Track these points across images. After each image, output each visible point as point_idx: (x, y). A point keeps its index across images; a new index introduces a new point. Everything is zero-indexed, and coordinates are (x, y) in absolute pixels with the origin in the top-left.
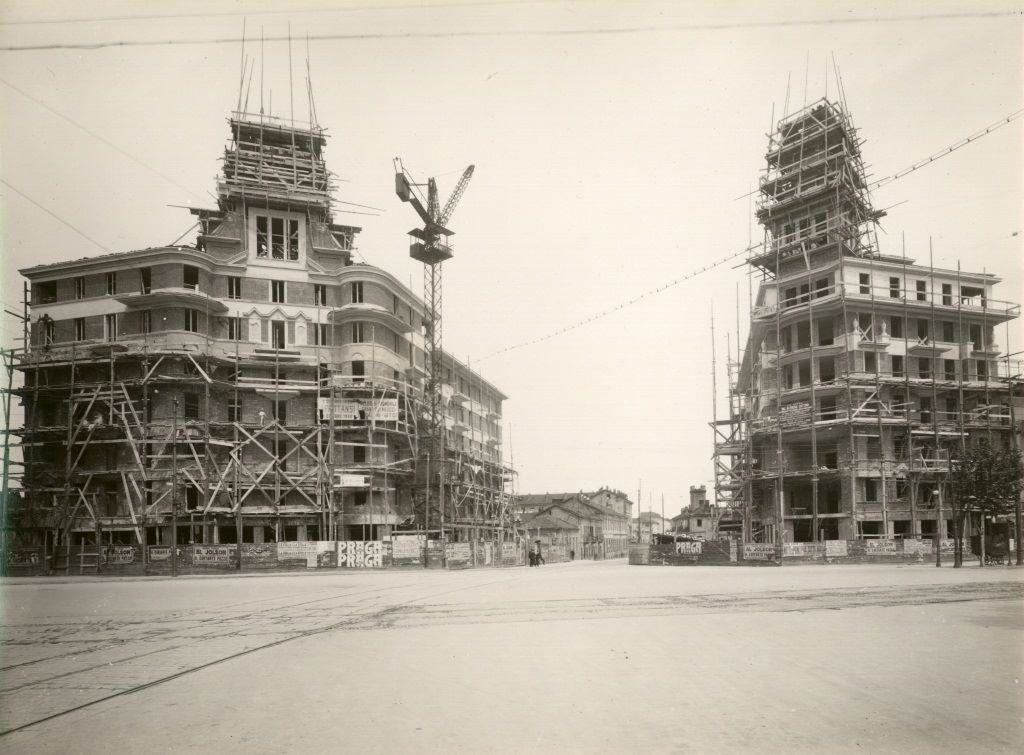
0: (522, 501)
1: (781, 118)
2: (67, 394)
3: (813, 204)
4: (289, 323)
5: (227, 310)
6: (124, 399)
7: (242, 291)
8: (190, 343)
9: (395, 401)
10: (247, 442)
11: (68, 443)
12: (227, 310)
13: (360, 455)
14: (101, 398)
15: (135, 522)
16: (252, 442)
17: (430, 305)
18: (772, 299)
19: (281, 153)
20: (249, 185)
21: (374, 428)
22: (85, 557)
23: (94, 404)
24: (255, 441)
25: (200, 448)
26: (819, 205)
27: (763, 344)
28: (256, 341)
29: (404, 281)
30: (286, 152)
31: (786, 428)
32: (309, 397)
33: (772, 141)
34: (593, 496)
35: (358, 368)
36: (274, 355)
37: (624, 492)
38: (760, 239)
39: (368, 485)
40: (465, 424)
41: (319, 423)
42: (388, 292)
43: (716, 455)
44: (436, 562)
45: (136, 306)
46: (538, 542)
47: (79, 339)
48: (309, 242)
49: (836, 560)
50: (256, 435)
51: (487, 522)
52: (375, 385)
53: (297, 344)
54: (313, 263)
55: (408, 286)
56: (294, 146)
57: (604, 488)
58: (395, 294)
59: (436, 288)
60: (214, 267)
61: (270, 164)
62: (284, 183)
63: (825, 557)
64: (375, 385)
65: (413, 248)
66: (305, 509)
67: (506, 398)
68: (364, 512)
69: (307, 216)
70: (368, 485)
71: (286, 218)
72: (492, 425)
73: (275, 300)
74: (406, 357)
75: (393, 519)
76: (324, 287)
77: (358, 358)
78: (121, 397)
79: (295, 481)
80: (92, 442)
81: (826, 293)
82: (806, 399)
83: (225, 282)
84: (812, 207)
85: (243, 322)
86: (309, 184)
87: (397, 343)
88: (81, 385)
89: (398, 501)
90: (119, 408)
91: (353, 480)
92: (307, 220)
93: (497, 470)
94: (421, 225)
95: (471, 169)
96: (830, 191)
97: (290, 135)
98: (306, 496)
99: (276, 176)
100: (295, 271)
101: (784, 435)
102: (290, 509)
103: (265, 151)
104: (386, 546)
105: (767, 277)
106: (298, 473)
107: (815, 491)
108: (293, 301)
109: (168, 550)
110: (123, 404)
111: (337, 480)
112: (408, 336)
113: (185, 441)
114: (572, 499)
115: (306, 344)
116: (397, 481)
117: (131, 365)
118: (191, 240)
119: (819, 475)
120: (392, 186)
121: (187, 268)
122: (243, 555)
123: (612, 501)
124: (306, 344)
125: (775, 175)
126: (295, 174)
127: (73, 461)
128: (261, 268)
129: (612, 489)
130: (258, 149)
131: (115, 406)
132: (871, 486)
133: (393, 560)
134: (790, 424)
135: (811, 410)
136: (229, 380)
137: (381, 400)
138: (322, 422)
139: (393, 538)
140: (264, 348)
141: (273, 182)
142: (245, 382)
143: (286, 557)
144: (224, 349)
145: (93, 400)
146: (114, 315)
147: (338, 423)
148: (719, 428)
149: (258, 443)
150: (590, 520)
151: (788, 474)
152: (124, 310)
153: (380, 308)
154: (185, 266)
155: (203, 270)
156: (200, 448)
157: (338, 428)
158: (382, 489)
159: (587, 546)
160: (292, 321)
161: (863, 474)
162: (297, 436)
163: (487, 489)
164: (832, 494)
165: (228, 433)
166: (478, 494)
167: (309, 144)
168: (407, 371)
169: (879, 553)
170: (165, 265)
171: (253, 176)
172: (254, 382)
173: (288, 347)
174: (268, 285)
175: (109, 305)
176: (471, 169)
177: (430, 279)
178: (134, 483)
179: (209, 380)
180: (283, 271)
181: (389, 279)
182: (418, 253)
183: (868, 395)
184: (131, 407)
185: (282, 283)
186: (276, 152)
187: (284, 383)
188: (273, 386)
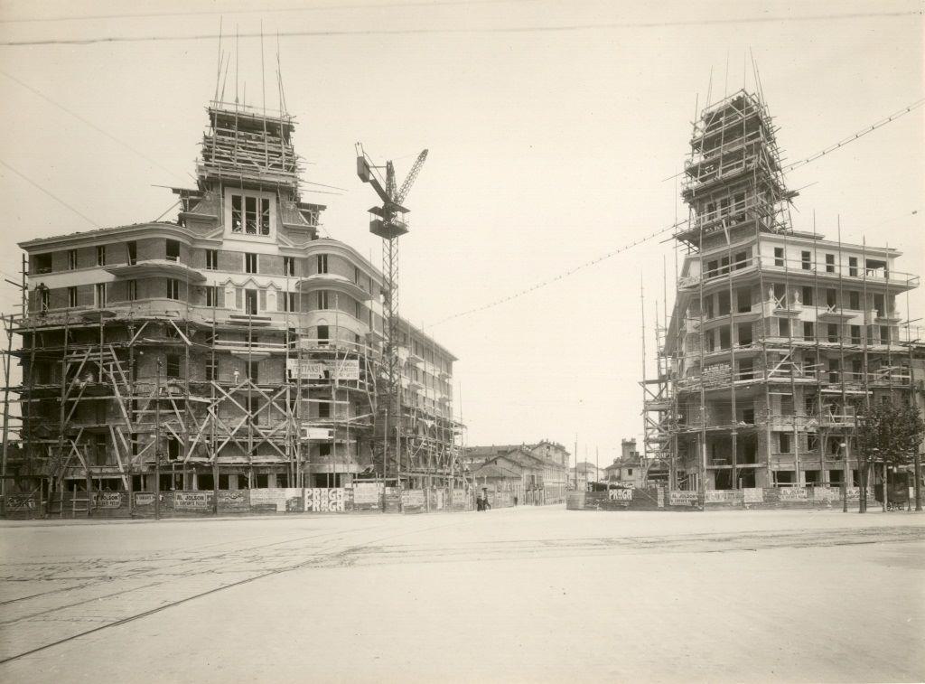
0: (470, 453)
2: (61, 355)
5: (205, 280)
9: (357, 362)
10: (223, 399)
11: (62, 399)
13: (324, 410)
17: (388, 276)
18: (696, 270)
25: (181, 404)
26: (738, 186)
27: (688, 312)
28: (232, 308)
29: (366, 256)
32: (278, 358)
33: (696, 128)
34: (534, 448)
35: (323, 332)
38: (685, 216)
39: (332, 437)
40: (419, 383)
43: (645, 411)
44: (393, 507)
46: (485, 489)
47: (72, 306)
48: (279, 219)
49: (753, 506)
50: (231, 393)
51: (439, 471)
52: (339, 347)
54: (284, 238)
55: (368, 259)
56: (266, 132)
57: (545, 441)
58: (357, 268)
60: (194, 241)
61: (243, 148)
62: (256, 165)
63: (743, 503)
64: (339, 347)
66: (275, 459)
67: (456, 359)
68: (328, 462)
70: (332, 437)
71: (259, 197)
72: (443, 383)
73: (248, 271)
75: (354, 468)
76: (292, 260)
78: (110, 358)
81: (744, 265)
82: (727, 362)
83: (204, 255)
84: (732, 188)
85: (220, 291)
86: (280, 166)
87: (357, 309)
88: (73, 347)
90: (107, 368)
92: (278, 199)
93: (448, 425)
94: (380, 204)
95: (425, 153)
96: (748, 173)
99: (249, 159)
100: (266, 245)
103: (239, 137)
104: (348, 492)
108: (264, 272)
110: (111, 364)
111: (304, 433)
113: (168, 398)
115: (276, 310)
117: (118, 329)
118: (173, 217)
119: (738, 430)
120: (353, 168)
121: (169, 241)
122: (219, 500)
123: (552, 452)
124: (276, 310)
125: (698, 159)
126: (267, 158)
127: (66, 415)
128: (236, 242)
130: (233, 135)
132: (784, 440)
133: (354, 505)
136: (207, 342)
138: (291, 381)
139: (355, 485)
141: (246, 165)
142: (221, 345)
143: (258, 502)
144: (202, 315)
145: (84, 361)
146: (103, 284)
147: (305, 381)
148: (648, 386)
149: (233, 400)
150: (532, 469)
151: (711, 428)
153: (343, 279)
156: (181, 404)
160: (264, 289)
161: (778, 428)
164: (750, 448)
165: (206, 391)
167: (279, 130)
169: (792, 500)
171: (229, 159)
173: (260, 313)
175: (100, 275)
176: (425, 153)
178: (121, 435)
179: (189, 343)
182: (377, 228)
183: (782, 357)
184: (119, 367)
185: (254, 256)
186: (250, 138)
187: (256, 346)
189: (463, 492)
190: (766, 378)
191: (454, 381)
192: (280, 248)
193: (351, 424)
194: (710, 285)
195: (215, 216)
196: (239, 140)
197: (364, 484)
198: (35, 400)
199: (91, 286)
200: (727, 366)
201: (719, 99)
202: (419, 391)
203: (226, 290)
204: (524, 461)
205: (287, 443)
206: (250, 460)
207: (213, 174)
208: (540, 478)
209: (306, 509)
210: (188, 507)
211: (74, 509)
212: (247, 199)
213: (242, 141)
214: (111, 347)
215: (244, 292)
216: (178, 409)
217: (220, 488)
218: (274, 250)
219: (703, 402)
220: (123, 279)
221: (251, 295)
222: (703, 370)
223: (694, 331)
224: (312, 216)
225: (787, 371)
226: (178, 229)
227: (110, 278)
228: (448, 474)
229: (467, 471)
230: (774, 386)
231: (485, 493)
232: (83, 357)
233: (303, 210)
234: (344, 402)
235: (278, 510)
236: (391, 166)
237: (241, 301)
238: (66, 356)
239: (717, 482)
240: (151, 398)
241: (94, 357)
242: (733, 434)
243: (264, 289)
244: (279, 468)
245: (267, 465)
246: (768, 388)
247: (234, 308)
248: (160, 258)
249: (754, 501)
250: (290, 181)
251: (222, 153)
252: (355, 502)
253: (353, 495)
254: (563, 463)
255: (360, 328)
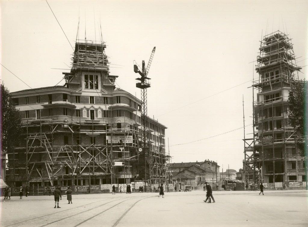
0: (174, 166)
1: (265, 35)
2: (25, 136)
3: (274, 67)
4: (96, 111)
5: (76, 107)
6: (45, 138)
7: (81, 100)
8: (66, 120)
9: (132, 136)
10: (84, 151)
11: (27, 153)
12: (76, 107)
13: (120, 155)
14: (37, 138)
15: (50, 179)
16: (85, 151)
17: (143, 101)
18: (262, 99)
19: (92, 53)
20: (83, 65)
21: (125, 146)
22: (39, 190)
23: (35, 140)
24: (86, 151)
25: (70, 154)
26: (276, 68)
27: (258, 114)
28: (86, 117)
29: (134, 94)
30: (94, 52)
31: (265, 144)
32: (104, 136)
33: (261, 43)
34: (201, 164)
35: (119, 126)
36: (92, 122)
37: (215, 161)
38: (257, 78)
39: (123, 165)
40: (133, 107)
41: (107, 145)
42: (127, 98)
43: (245, 152)
44: (149, 190)
45: (47, 107)
46: (180, 184)
47: (27, 118)
48: (102, 83)
49: (278, 189)
50: (86, 149)
51: (161, 176)
52: (125, 131)
53: (98, 118)
54: (103, 90)
55: (134, 95)
56: (96, 50)
57: (207, 160)
58: (130, 99)
59: (145, 98)
60: (72, 93)
61: (88, 57)
62: (94, 63)
63: (274, 188)
64: (125, 131)
65: (137, 84)
66: (102, 174)
67: (166, 128)
68: (122, 174)
69: (101, 73)
70: (123, 165)
71: (94, 74)
72: (161, 140)
73: (91, 103)
74: (134, 120)
75: (131, 176)
76: (107, 98)
77: (119, 122)
78: (44, 138)
79: (99, 164)
80: (35, 153)
81: (279, 99)
82: (271, 135)
83: (75, 98)
84: (274, 68)
85: (80, 111)
86: (102, 63)
87: (131, 116)
88: (31, 134)
89: (132, 171)
90: (43, 141)
91: (118, 164)
92: (101, 75)
93: (164, 157)
94: (140, 77)
95: (155, 48)
96: (279, 64)
97: (95, 46)
98: (103, 169)
99: (91, 61)
100: (96, 93)
101: (264, 146)
102: (98, 174)
103: (87, 53)
104: (133, 185)
105: (260, 89)
106: (100, 162)
107: (274, 166)
108: (97, 103)
109: (67, 187)
110: (45, 140)
111: (114, 164)
112: (134, 113)
113: (66, 152)
114: (193, 166)
115: (101, 117)
116: (132, 163)
117: (47, 128)
118: (63, 83)
119: (275, 161)
120: (133, 69)
121: (64, 94)
122: (91, 188)
123: (210, 166)
124: (101, 117)
125: (264, 55)
126: (97, 60)
127: (28, 159)
128: (87, 92)
129: (210, 160)
130: (84, 52)
131: (42, 141)
132: (293, 164)
133: (135, 190)
134: (266, 143)
135: (272, 139)
136: (77, 130)
137: (128, 136)
138: (108, 144)
139: (135, 183)
140: (88, 120)
141: (89, 63)
142: (82, 131)
143: (104, 189)
144: (75, 120)
145: (35, 139)
146: (39, 110)
147: (113, 144)
148: (246, 141)
149: (87, 152)
150: (200, 175)
151: (266, 160)
152: (43, 108)
153: (126, 105)
154: (63, 94)
155: (69, 94)
156: (70, 154)
157: (114, 146)
158: (128, 166)
159: (199, 185)
160: (97, 110)
161: (290, 160)
162: (100, 149)
163: (161, 164)
164: (280, 167)
165: (78, 149)
166: (158, 166)
167: (100, 48)
168: (134, 125)
169: (294, 186)
170: (57, 94)
171: (83, 62)
172: (85, 131)
173: (96, 119)
174: (88, 98)
175: (39, 106)
176: (155, 48)
177: (143, 95)
178: (49, 166)
179: (73, 132)
180: (93, 93)
181: (129, 95)
182: (138, 85)
183: (292, 133)
184: (48, 141)
185: (93, 97)
186: (91, 53)
187: (94, 131)
188: (92, 132)
189: (172, 185)
190: (285, 142)
191: (166, 138)
192: (102, 94)
193: (130, 160)
194: (265, 106)
195: (79, 83)
196: (87, 54)
197: (3, 172)
198: (16, 153)
199: (35, 110)
200: (271, 137)
201: (270, 32)
202: (152, 144)
203: (83, 111)
204: (196, 171)
205: (107, 167)
206: (93, 174)
207: (79, 68)
208: (204, 178)
209: (119, 191)
210: (80, 191)
211: (38, 193)
212: (90, 76)
213: (88, 54)
214: (44, 133)
215: (90, 111)
216: (70, 156)
217: (78, 185)
218: (100, 95)
219: (263, 150)
220: (47, 108)
221: (92, 112)
222: (263, 138)
223: (260, 122)
224: (113, 80)
225: (293, 139)
226: (67, 90)
227: (42, 108)
228: (164, 178)
229: (172, 176)
230: (288, 145)
231: (180, 185)
232: (34, 137)
233: (110, 78)
234: (128, 152)
235: (110, 192)
236: (144, 62)
237: (89, 115)
238: (27, 137)
239: (290, 178)
240: (60, 152)
241: (38, 137)
242: (274, 162)
243: (97, 110)
244: (103, 176)
245: (100, 176)
246: (285, 145)
247: (86, 117)
248: (61, 100)
249: (279, 187)
250: (106, 69)
251: (81, 59)
252: (136, 189)
253: (135, 186)
254: (216, 171)
255: (132, 122)
